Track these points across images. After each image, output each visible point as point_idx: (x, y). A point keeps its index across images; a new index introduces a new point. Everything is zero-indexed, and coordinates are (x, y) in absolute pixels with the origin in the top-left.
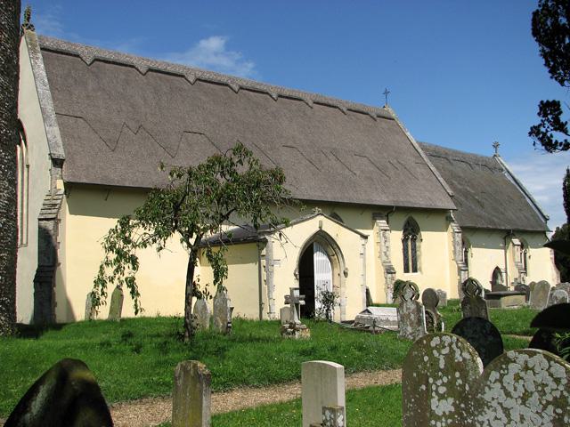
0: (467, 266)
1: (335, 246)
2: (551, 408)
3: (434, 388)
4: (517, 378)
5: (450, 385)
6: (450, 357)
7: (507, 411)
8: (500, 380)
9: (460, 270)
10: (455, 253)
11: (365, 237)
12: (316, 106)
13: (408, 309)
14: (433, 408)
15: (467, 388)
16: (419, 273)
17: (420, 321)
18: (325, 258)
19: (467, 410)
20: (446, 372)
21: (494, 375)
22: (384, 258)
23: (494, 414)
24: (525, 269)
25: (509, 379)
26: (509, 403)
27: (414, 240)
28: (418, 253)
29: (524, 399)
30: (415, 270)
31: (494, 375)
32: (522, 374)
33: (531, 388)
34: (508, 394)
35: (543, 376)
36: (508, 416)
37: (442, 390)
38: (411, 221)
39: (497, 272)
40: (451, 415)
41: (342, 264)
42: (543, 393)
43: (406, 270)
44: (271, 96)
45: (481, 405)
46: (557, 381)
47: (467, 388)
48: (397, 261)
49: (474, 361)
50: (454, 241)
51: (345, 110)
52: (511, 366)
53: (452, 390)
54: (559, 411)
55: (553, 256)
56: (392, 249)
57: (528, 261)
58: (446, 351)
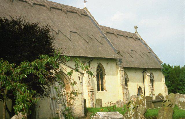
30: (102, 90)
43: (98, 90)
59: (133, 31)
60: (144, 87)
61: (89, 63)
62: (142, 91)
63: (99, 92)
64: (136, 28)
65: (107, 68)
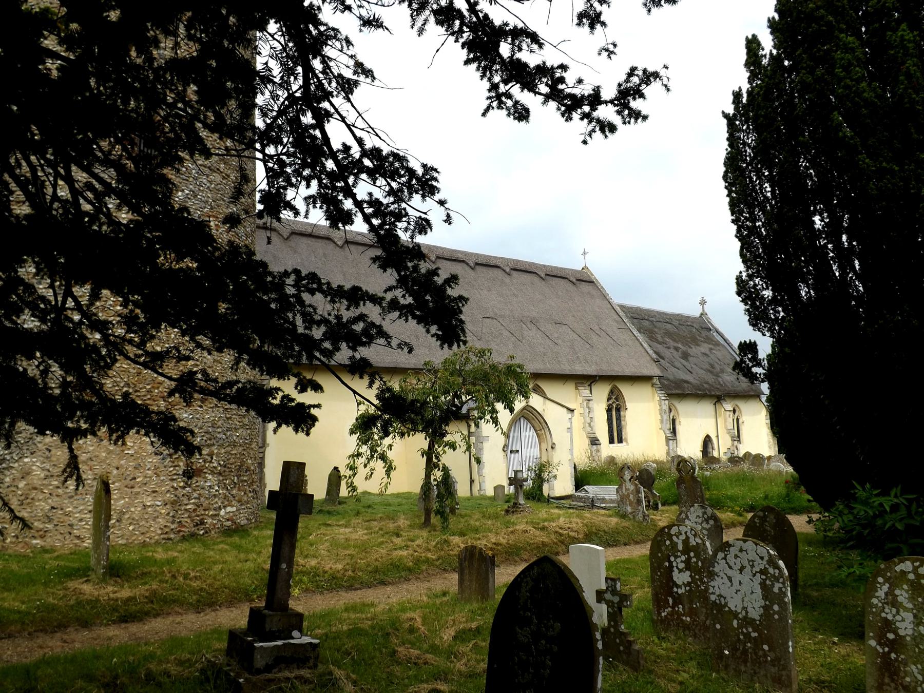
0: (675, 435)
1: (544, 424)
2: (758, 575)
3: (675, 564)
4: (736, 556)
5: (687, 562)
6: (686, 541)
7: (730, 579)
8: (725, 558)
9: (668, 440)
10: (662, 421)
11: (572, 411)
12: (514, 273)
13: (627, 490)
14: (675, 579)
15: (700, 564)
16: (624, 443)
17: (639, 502)
18: (533, 433)
19: (701, 580)
20: (683, 553)
21: (721, 555)
22: (589, 429)
23: (722, 581)
24: (739, 436)
25: (731, 558)
26: (730, 573)
27: (618, 410)
28: (623, 423)
29: (742, 569)
30: (620, 441)
31: (721, 555)
32: (739, 554)
33: (746, 563)
34: (730, 567)
35: (752, 555)
36: (731, 581)
37: (681, 566)
38: (615, 382)
39: (707, 441)
40: (689, 584)
41: (549, 439)
42: (752, 566)
43: (611, 441)
44: (467, 264)
45: (712, 575)
46: (762, 558)
47: (700, 564)
48: (602, 433)
49: (704, 545)
50: (660, 410)
51: (543, 276)
52: (731, 549)
53: (688, 566)
54: (764, 577)
55: (769, 421)
56: (596, 420)
57: (742, 428)
58: (683, 537)
59: (693, 311)
60: (717, 436)
61: (590, 385)
62: (712, 444)
63: (611, 445)
64: (703, 303)
65: (627, 391)
